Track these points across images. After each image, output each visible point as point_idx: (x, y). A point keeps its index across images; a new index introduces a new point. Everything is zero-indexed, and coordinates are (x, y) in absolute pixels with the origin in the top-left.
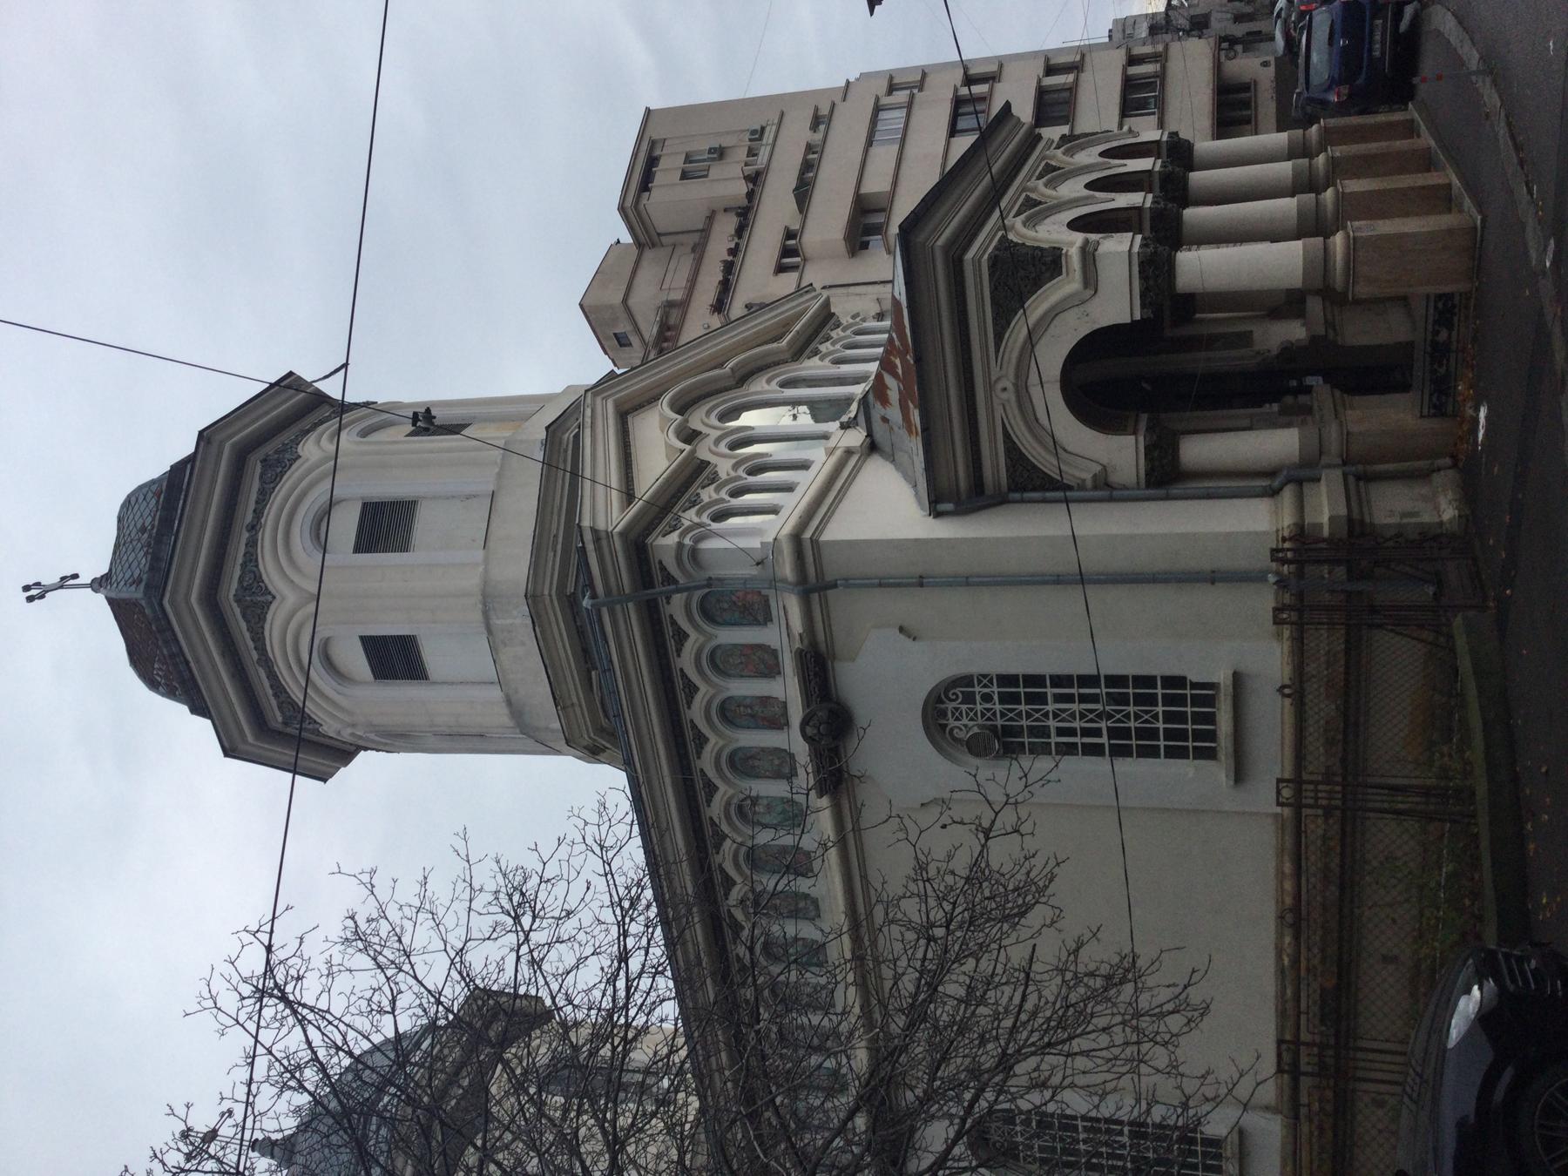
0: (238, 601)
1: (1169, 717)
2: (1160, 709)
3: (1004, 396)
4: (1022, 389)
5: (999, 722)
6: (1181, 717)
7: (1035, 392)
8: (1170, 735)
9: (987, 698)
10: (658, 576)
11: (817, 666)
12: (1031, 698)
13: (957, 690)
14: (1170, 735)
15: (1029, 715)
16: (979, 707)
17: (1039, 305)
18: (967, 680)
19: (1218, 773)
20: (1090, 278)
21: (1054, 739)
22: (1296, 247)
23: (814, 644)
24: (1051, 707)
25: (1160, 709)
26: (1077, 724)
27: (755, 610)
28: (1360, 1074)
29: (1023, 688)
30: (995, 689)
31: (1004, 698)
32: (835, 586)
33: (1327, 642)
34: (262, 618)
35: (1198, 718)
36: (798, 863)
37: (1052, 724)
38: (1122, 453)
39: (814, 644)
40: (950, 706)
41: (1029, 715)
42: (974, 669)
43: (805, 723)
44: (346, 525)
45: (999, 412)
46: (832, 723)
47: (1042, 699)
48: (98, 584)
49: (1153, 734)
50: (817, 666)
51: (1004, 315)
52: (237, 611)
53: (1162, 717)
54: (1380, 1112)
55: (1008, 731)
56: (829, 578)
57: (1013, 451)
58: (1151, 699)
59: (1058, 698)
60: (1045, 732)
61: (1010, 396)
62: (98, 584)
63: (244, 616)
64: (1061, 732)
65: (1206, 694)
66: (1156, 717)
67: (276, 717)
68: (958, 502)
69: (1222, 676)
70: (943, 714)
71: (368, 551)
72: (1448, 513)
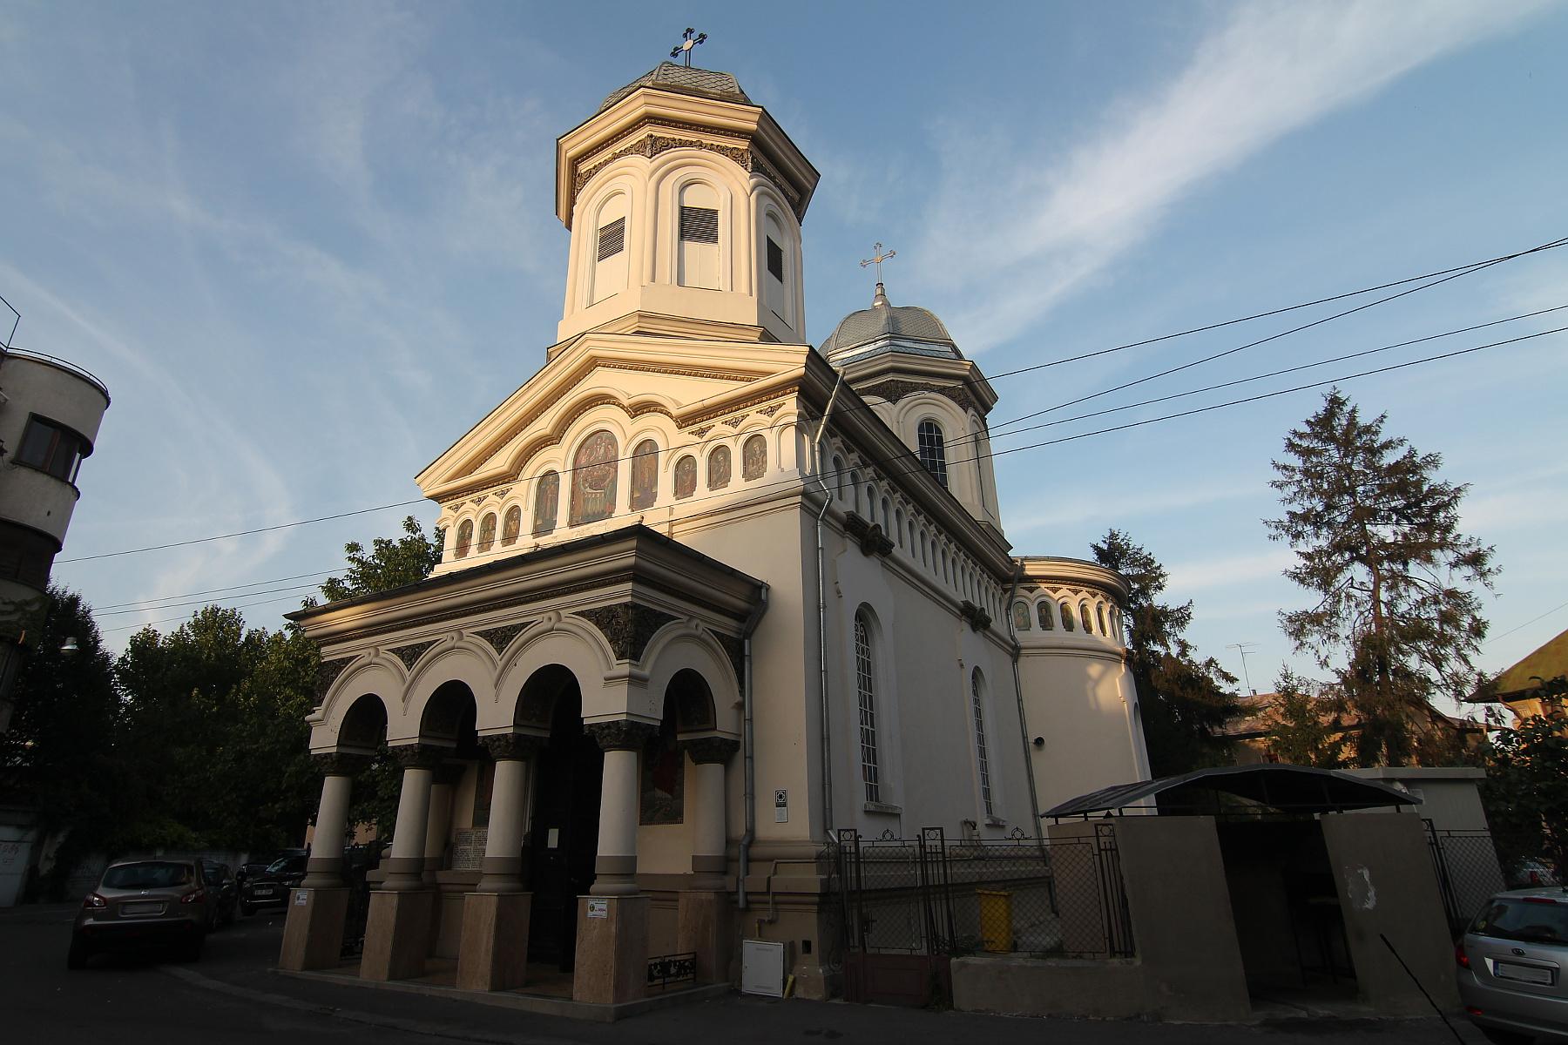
44: (694, 199)
67: (584, 168)
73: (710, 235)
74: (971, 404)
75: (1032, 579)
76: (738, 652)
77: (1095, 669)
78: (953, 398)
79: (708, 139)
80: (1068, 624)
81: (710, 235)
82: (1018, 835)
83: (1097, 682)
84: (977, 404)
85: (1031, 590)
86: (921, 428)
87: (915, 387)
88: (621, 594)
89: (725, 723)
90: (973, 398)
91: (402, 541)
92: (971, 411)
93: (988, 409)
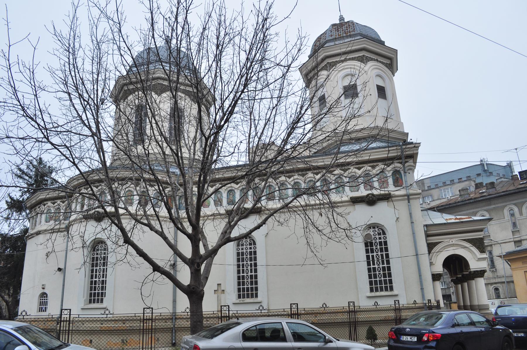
0: (363, 55)
1: (98, 293)
2: (383, 279)
3: (451, 241)
4: (453, 245)
5: (374, 241)
6: (98, 296)
7: (452, 248)
8: (95, 293)
10: (406, 160)
13: (381, 231)
14: (376, 281)
15: (377, 248)
16: (377, 236)
17: (474, 249)
18: (384, 233)
19: (82, 306)
20: (480, 259)
21: (385, 265)
22: (462, 304)
23: (392, 197)
25: (383, 279)
26: (98, 273)
27: (398, 182)
28: (145, 335)
29: (384, 246)
30: (383, 240)
31: (251, 252)
32: (409, 202)
33: (345, 317)
34: (359, 61)
35: (98, 299)
37: (98, 268)
38: (439, 268)
39: (392, 197)
40: (377, 229)
41: (377, 248)
42: (387, 236)
43: (373, 195)
44: (381, 84)
45: (446, 240)
46: (371, 201)
48: (341, 18)
49: (95, 290)
50: (387, 197)
51: (471, 241)
52: (360, 55)
53: (381, 279)
54: (93, 341)
55: (371, 244)
56: (411, 201)
58: (252, 284)
60: (251, 276)
61: (451, 243)
62: (341, 18)
63: (360, 56)
64: (96, 270)
65: (392, 289)
66: (380, 278)
68: (427, 231)
69: (395, 292)
72: (416, 340)
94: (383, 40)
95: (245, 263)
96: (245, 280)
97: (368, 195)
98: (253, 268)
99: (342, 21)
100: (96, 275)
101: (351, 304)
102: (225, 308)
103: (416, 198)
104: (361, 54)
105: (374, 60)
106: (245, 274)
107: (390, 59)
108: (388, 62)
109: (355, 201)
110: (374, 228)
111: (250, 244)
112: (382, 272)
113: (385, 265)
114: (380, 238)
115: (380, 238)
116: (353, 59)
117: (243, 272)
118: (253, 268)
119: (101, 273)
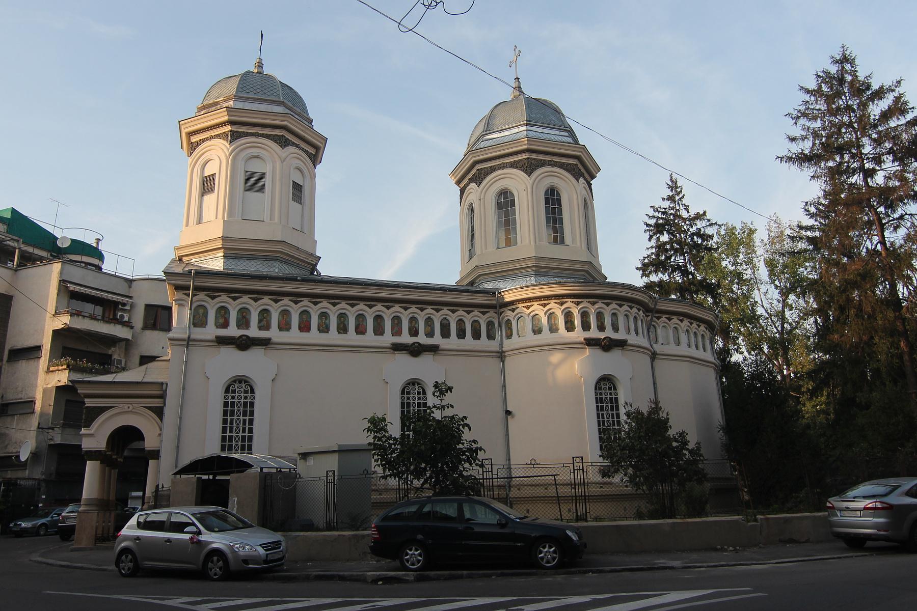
9: (233, 397)
11: (265, 343)
12: (612, 406)
18: (252, 391)
21: (247, 434)
24: (241, 418)
29: (249, 408)
36: (324, 328)
37: (241, 434)
40: (243, 385)
44: (256, 167)
47: (612, 410)
50: (265, 343)
57: (103, 410)
59: (613, 415)
70: (240, 382)
71: (246, 176)
73: (261, 189)
74: (582, 175)
75: (512, 303)
76: (159, 412)
77: (556, 357)
78: (567, 170)
79: (262, 131)
80: (537, 331)
81: (261, 189)
82: (533, 462)
83: (557, 366)
84: (586, 175)
85: (513, 310)
86: (546, 193)
87: (493, 169)
88: (228, 128)
89: (149, 444)
90: (583, 170)
91: (676, 235)
92: (581, 179)
93: (593, 177)
94: (311, 116)
95: (605, 412)
96: (234, 443)
97: (414, 343)
98: (247, 425)
99: (260, 70)
100: (613, 418)
101: (331, 474)
102: (487, 462)
103: (196, 346)
104: (280, 133)
105: (297, 146)
106: (234, 435)
107: (317, 148)
108: (312, 151)
109: (222, 341)
110: (414, 384)
111: (419, 393)
112: (240, 443)
113: (247, 434)
114: (246, 398)
115: (611, 394)
116: (268, 137)
117: (231, 431)
118: (247, 425)
119: (241, 426)
